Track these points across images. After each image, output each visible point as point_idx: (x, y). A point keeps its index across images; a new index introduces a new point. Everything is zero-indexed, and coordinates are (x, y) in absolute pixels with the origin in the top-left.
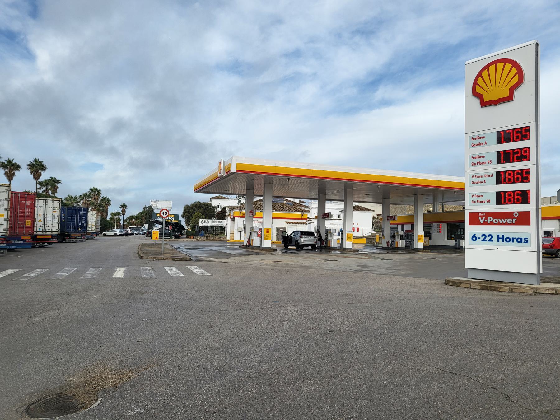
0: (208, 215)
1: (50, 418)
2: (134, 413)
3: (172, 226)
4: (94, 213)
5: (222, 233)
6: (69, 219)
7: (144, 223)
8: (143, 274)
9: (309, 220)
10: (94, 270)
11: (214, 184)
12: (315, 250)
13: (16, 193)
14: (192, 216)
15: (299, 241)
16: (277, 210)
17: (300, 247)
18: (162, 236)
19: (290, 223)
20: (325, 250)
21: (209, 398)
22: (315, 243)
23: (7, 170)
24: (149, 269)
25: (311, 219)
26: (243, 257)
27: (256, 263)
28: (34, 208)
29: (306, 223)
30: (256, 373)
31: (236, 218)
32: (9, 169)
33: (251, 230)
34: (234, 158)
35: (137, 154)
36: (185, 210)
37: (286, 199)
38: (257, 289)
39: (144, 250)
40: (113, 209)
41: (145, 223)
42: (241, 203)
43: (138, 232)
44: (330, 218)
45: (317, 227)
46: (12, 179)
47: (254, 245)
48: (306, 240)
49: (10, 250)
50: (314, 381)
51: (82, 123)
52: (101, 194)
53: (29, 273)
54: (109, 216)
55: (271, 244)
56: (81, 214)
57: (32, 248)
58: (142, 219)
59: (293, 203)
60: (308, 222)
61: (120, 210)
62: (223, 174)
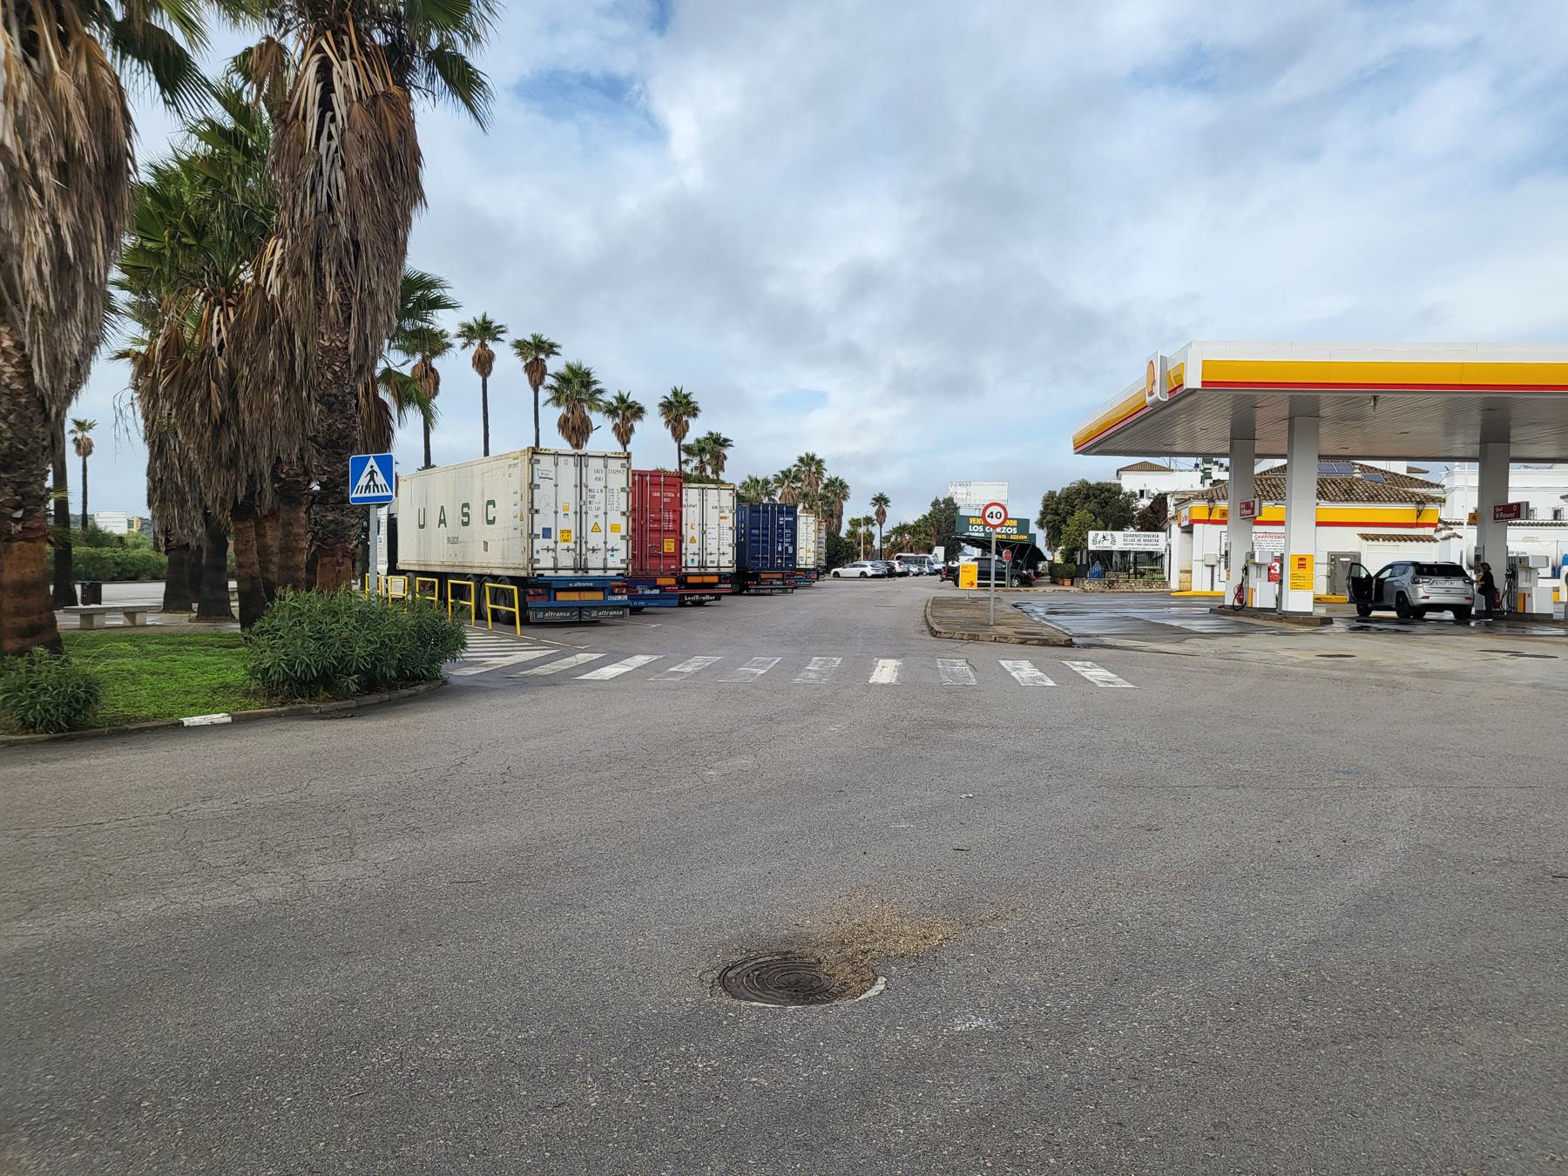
0: (1113, 518)
1: (773, 1006)
2: (970, 1027)
3: (1012, 551)
4: (811, 519)
5: (1154, 570)
6: (755, 535)
7: (934, 543)
8: (944, 678)
9: (1441, 529)
10: (823, 662)
11: (1132, 427)
12: (1468, 624)
13: (642, 474)
14: (1065, 521)
15: (1410, 594)
16: (1330, 499)
17: (1411, 614)
18: (989, 579)
19: (1376, 538)
20: (1504, 624)
21: (1171, 1021)
22: (1467, 602)
23: (617, 421)
24: (960, 666)
25: (1450, 524)
26: (1226, 638)
27: (1270, 657)
28: (678, 509)
29: (1430, 539)
30: (1309, 972)
31: (1197, 527)
32: (621, 416)
33: (1247, 561)
34: (1193, 344)
35: (912, 357)
36: (1046, 507)
37: (1361, 465)
38: (1279, 731)
39: (940, 615)
40: (855, 508)
41: (938, 545)
42: (1211, 481)
43: (919, 569)
44: (1527, 519)
45: (1476, 549)
46: (628, 442)
47: (1258, 606)
48: (1434, 590)
49: (636, 611)
50: (1517, 1024)
51: (774, 286)
52: (825, 469)
53: (680, 665)
54: (845, 528)
55: (1314, 602)
56: (781, 523)
57: (679, 606)
58: (928, 535)
59: (1386, 476)
60: (1438, 536)
61: (871, 512)
62: (1160, 395)
